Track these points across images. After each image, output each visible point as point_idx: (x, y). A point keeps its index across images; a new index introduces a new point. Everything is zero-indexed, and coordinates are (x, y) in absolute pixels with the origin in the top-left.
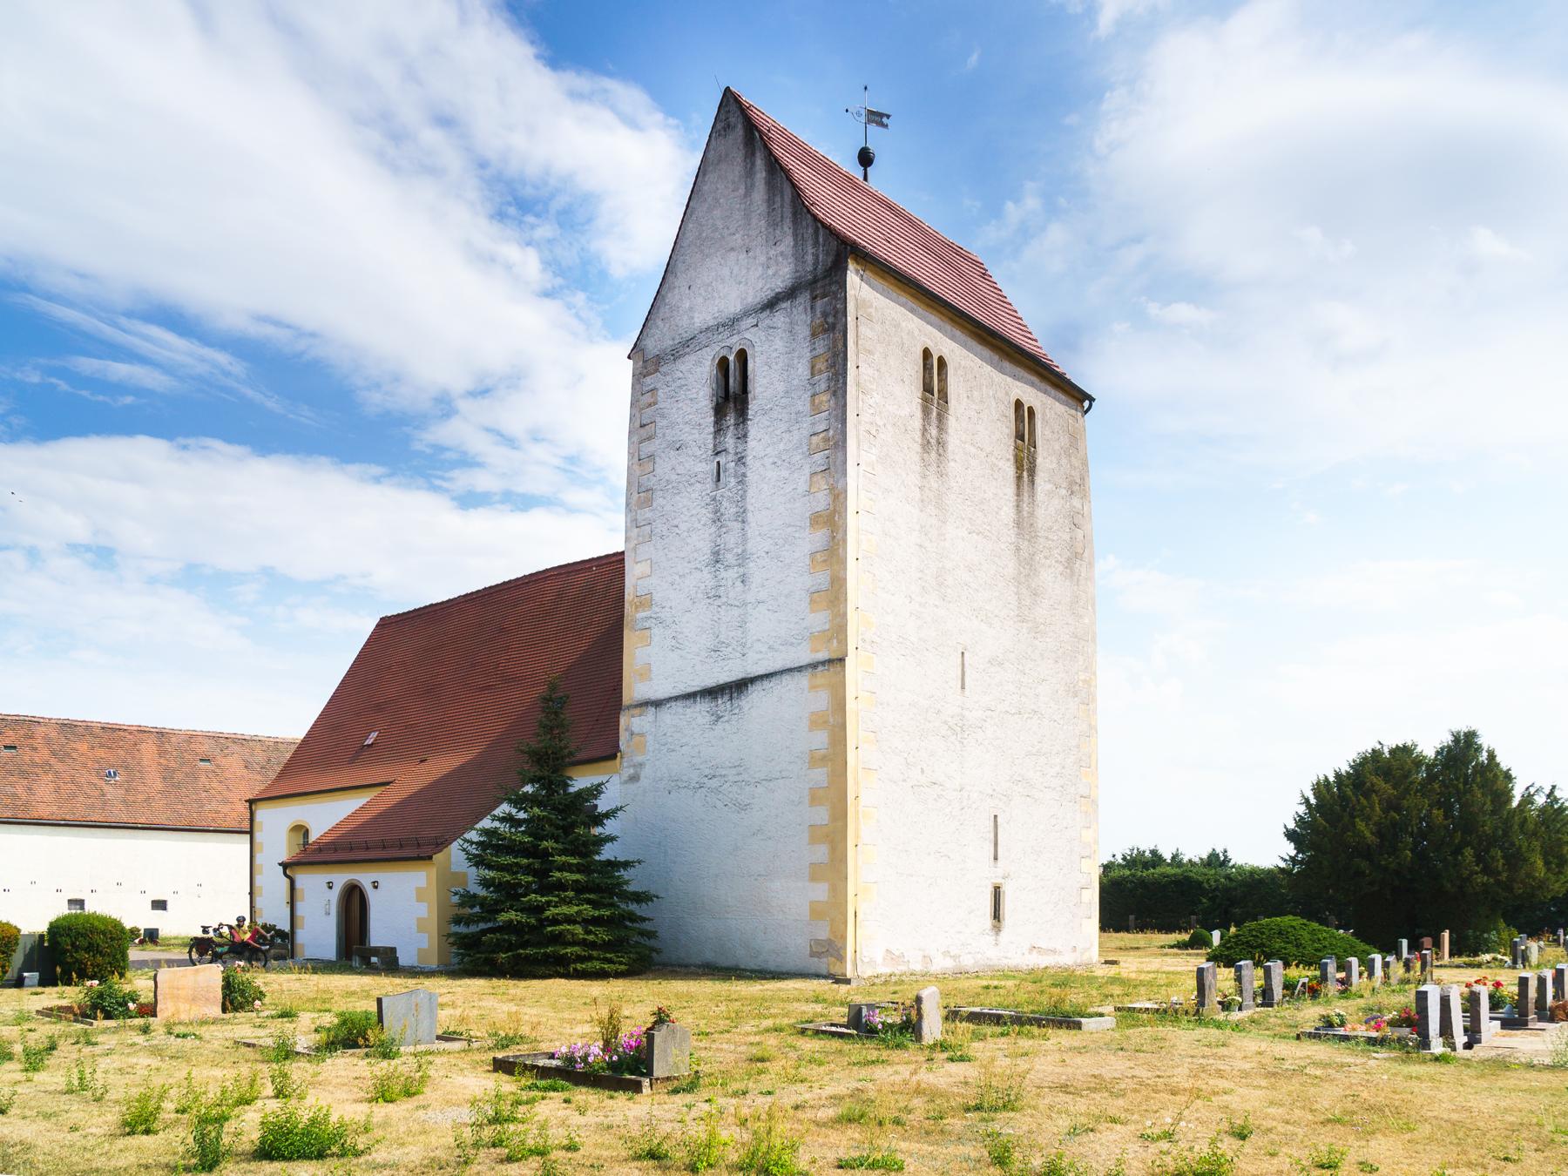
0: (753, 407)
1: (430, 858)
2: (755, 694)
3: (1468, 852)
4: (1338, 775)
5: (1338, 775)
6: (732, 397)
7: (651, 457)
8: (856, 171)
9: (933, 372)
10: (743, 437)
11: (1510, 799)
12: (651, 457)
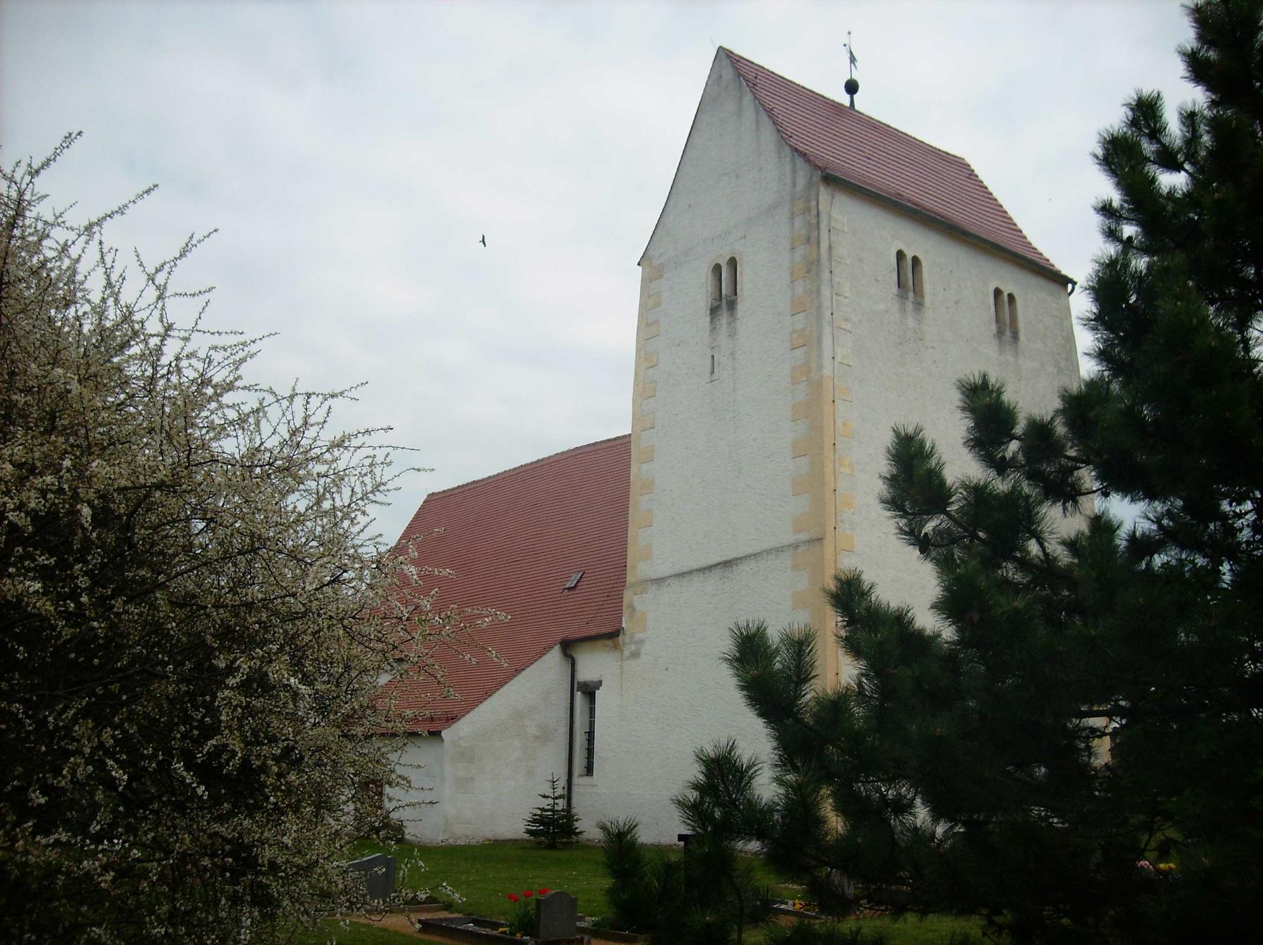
0: (740, 307)
1: (436, 734)
2: (744, 567)
3: (179, 766)
4: (696, 786)
5: (696, 786)
6: (724, 302)
7: (656, 322)
8: (844, 99)
9: (908, 273)
10: (732, 335)
11: (834, 794)
12: (656, 322)
